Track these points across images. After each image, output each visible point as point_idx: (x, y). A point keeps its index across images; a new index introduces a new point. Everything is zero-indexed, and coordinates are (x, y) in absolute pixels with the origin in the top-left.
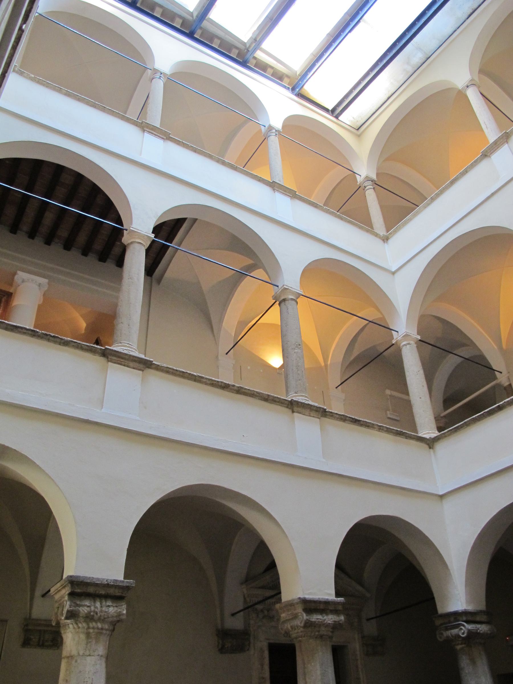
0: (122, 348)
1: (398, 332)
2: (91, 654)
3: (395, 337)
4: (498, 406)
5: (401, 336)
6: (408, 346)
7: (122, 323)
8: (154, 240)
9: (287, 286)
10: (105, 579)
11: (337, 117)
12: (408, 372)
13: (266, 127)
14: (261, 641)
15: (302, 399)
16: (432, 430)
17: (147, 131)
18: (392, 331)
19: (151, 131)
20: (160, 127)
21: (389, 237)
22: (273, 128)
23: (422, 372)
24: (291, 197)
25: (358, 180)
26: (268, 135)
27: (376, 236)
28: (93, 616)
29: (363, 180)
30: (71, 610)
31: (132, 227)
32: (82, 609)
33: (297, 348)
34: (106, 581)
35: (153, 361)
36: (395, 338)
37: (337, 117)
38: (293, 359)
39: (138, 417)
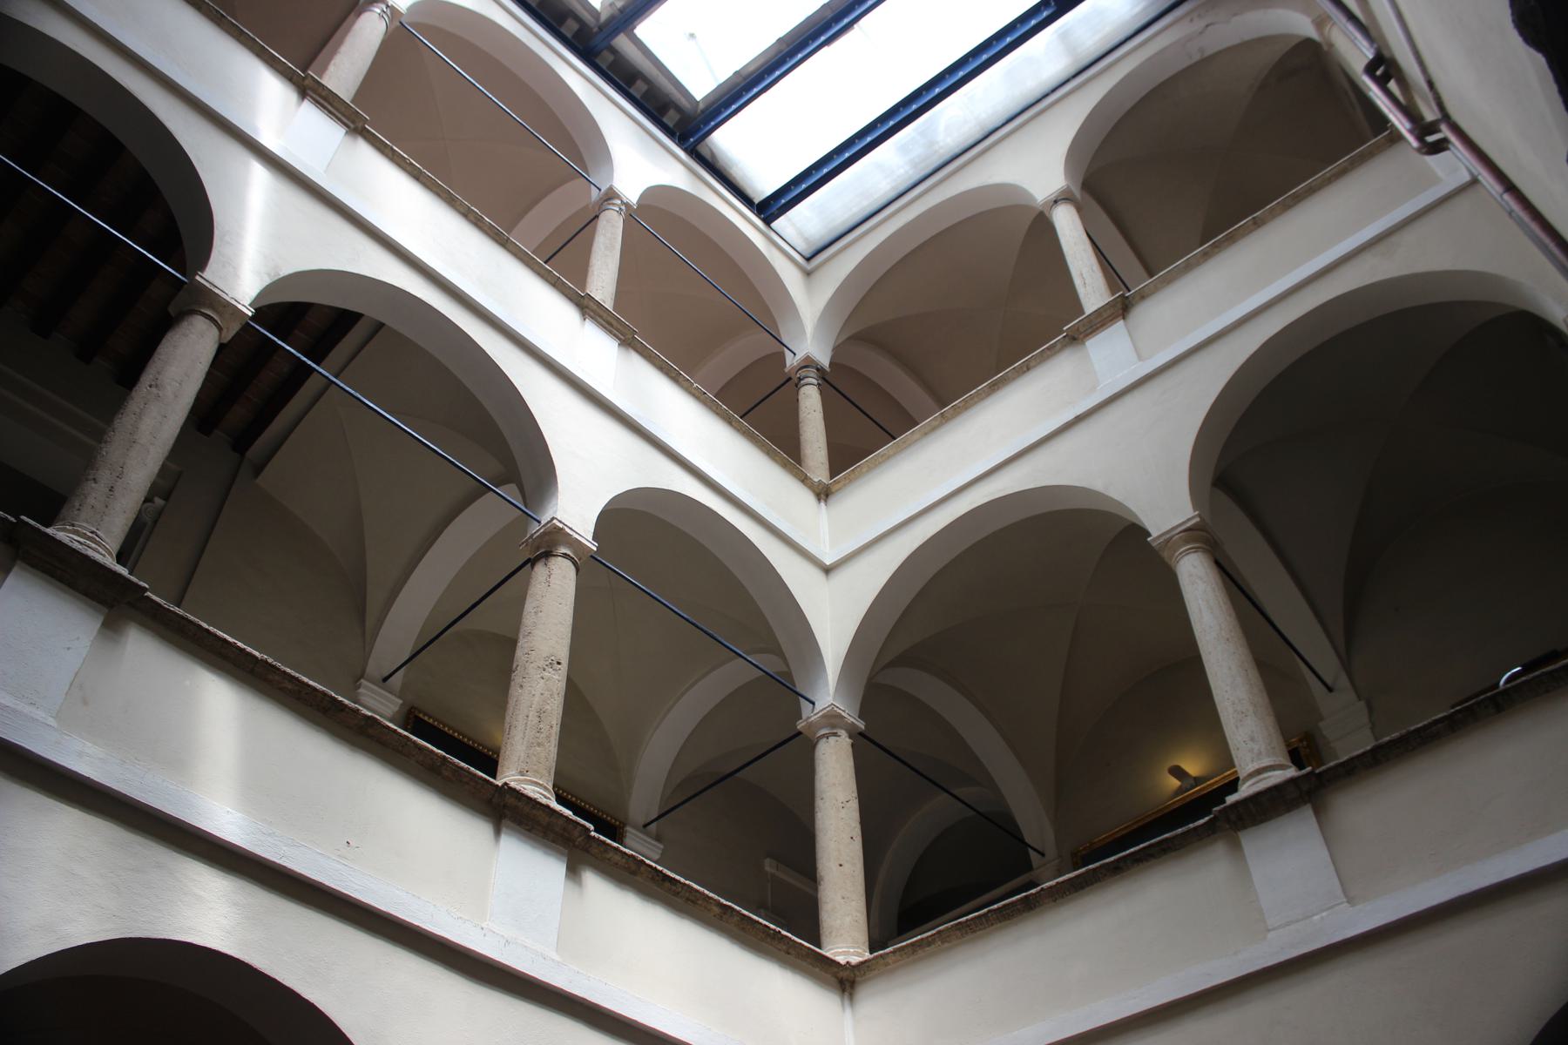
0: (71, 535)
4: (1026, 897)
5: (821, 714)
6: (832, 739)
7: (94, 479)
8: (248, 324)
9: (560, 522)
11: (768, 221)
13: (602, 191)
15: (534, 791)
16: (858, 947)
17: (311, 97)
18: (800, 698)
19: (322, 101)
20: (352, 102)
21: (833, 490)
22: (618, 197)
23: (854, 805)
24: (620, 339)
25: (788, 363)
26: (604, 208)
27: (803, 481)
29: (798, 364)
31: (201, 277)
33: (551, 670)
35: (145, 590)
36: (804, 716)
37: (768, 221)
38: (533, 693)
39: (51, 719)
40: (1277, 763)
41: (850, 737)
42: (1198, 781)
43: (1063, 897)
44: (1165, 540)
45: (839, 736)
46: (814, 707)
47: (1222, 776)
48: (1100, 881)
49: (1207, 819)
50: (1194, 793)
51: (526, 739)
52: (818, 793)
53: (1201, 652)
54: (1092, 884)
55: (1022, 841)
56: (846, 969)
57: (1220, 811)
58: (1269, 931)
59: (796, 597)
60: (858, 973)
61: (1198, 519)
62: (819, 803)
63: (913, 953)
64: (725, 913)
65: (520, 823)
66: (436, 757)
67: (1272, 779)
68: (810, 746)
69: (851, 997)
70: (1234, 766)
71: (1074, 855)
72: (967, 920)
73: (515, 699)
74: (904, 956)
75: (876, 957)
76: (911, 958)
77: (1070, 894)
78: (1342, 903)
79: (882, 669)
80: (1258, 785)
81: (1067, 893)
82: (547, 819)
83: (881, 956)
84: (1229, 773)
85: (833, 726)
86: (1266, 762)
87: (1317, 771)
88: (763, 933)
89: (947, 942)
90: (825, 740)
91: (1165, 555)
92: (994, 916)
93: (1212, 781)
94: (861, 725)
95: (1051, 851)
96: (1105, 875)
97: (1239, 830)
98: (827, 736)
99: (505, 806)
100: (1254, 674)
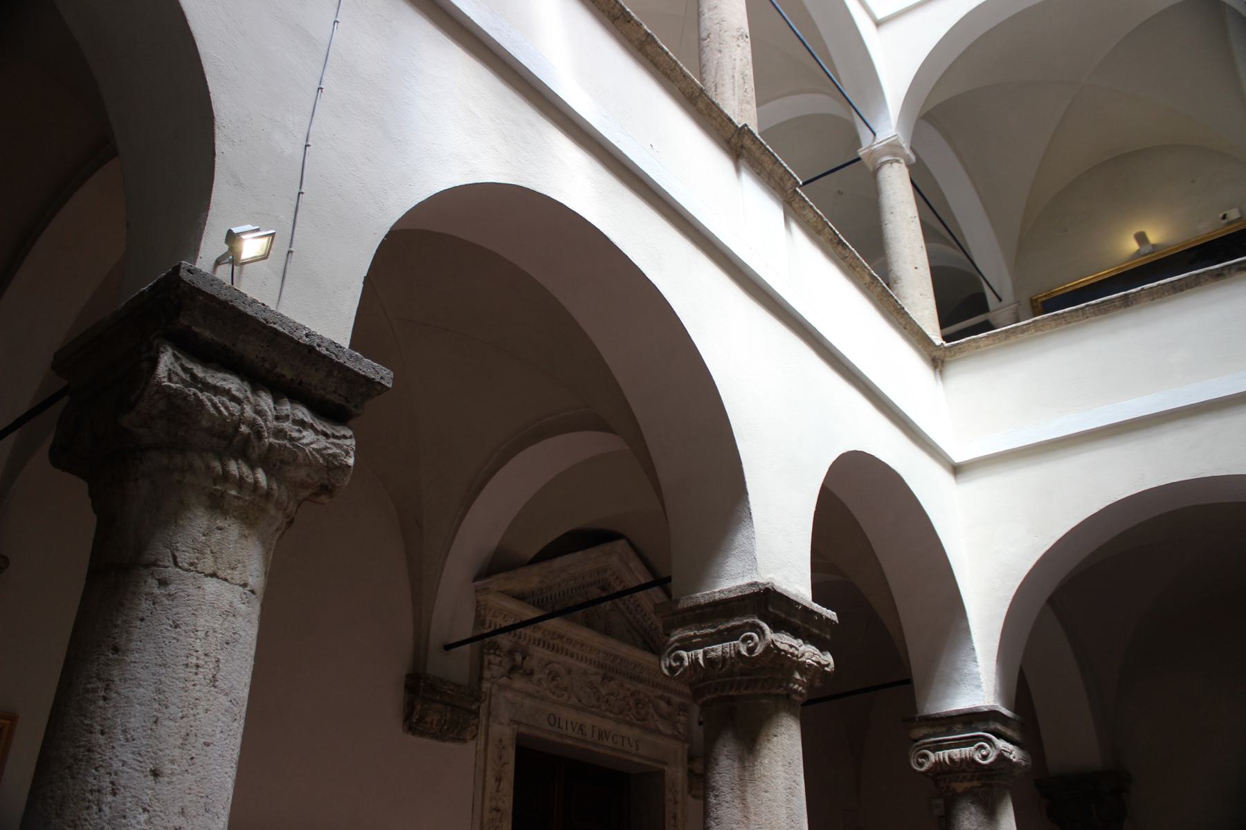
2: (220, 573)
4: (1125, 295)
6: (895, 165)
10: (305, 328)
14: (501, 723)
28: (247, 439)
30: (170, 387)
32: (211, 400)
34: (307, 335)
43: (1161, 297)
46: (874, 140)
51: (736, 96)
54: (1192, 287)
56: (941, 349)
59: (956, 22)
63: (1006, 339)
64: (872, 283)
65: (752, 166)
66: (695, 87)
68: (875, 172)
69: (941, 372)
71: (1032, 301)
72: (1064, 313)
73: (715, 62)
74: (997, 341)
77: (1169, 295)
82: (771, 167)
83: (974, 339)
85: (895, 155)
88: (893, 306)
90: (889, 165)
92: (1092, 310)
93: (1102, 273)
96: (1207, 280)
98: (891, 162)
99: (742, 147)
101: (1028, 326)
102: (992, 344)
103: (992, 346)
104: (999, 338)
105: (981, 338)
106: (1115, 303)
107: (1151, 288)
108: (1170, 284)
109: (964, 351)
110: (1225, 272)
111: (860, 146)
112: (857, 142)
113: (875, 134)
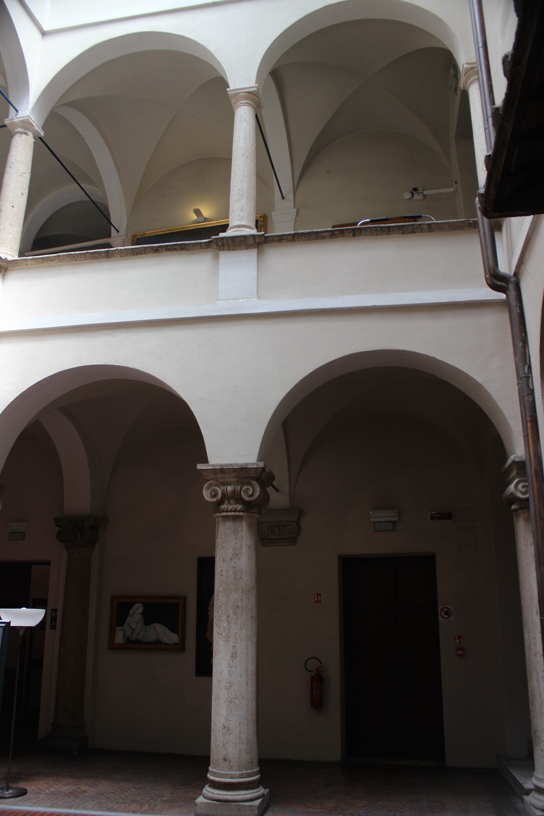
1: (17, 111)
3: (11, 117)
4: (108, 251)
5: (20, 119)
6: (24, 136)
12: (10, 167)
23: (28, 176)
36: (10, 117)
40: (249, 225)
41: (34, 138)
42: (206, 220)
43: (126, 256)
44: (236, 93)
45: (28, 135)
47: (218, 221)
48: (147, 254)
49: (207, 240)
50: (201, 225)
52: (9, 164)
53: (233, 158)
54: (142, 254)
55: (110, 222)
56: (4, 261)
57: (215, 239)
58: (218, 300)
60: (10, 265)
61: (256, 89)
62: (8, 169)
67: (244, 232)
68: (11, 136)
70: (228, 218)
71: (134, 236)
72: (75, 254)
74: (37, 263)
75: (22, 260)
76: (41, 265)
78: (255, 297)
79: (61, 106)
80: (237, 232)
81: (129, 255)
83: (25, 259)
84: (222, 221)
85: (26, 129)
86: (244, 223)
87: (266, 235)
89: (61, 261)
90: (19, 135)
91: (233, 101)
92: (89, 256)
93: (213, 222)
94: (42, 133)
95: (123, 231)
96: (150, 252)
97: (220, 251)
98: (21, 133)
100: (254, 179)
101: (55, 258)
102: (34, 264)
103: (34, 265)
104: (38, 262)
105: (28, 259)
106: (102, 254)
107: (121, 250)
108: (131, 250)
109: (19, 265)
110: (160, 249)
111: (7, 117)
112: (7, 115)
113: (17, 111)
